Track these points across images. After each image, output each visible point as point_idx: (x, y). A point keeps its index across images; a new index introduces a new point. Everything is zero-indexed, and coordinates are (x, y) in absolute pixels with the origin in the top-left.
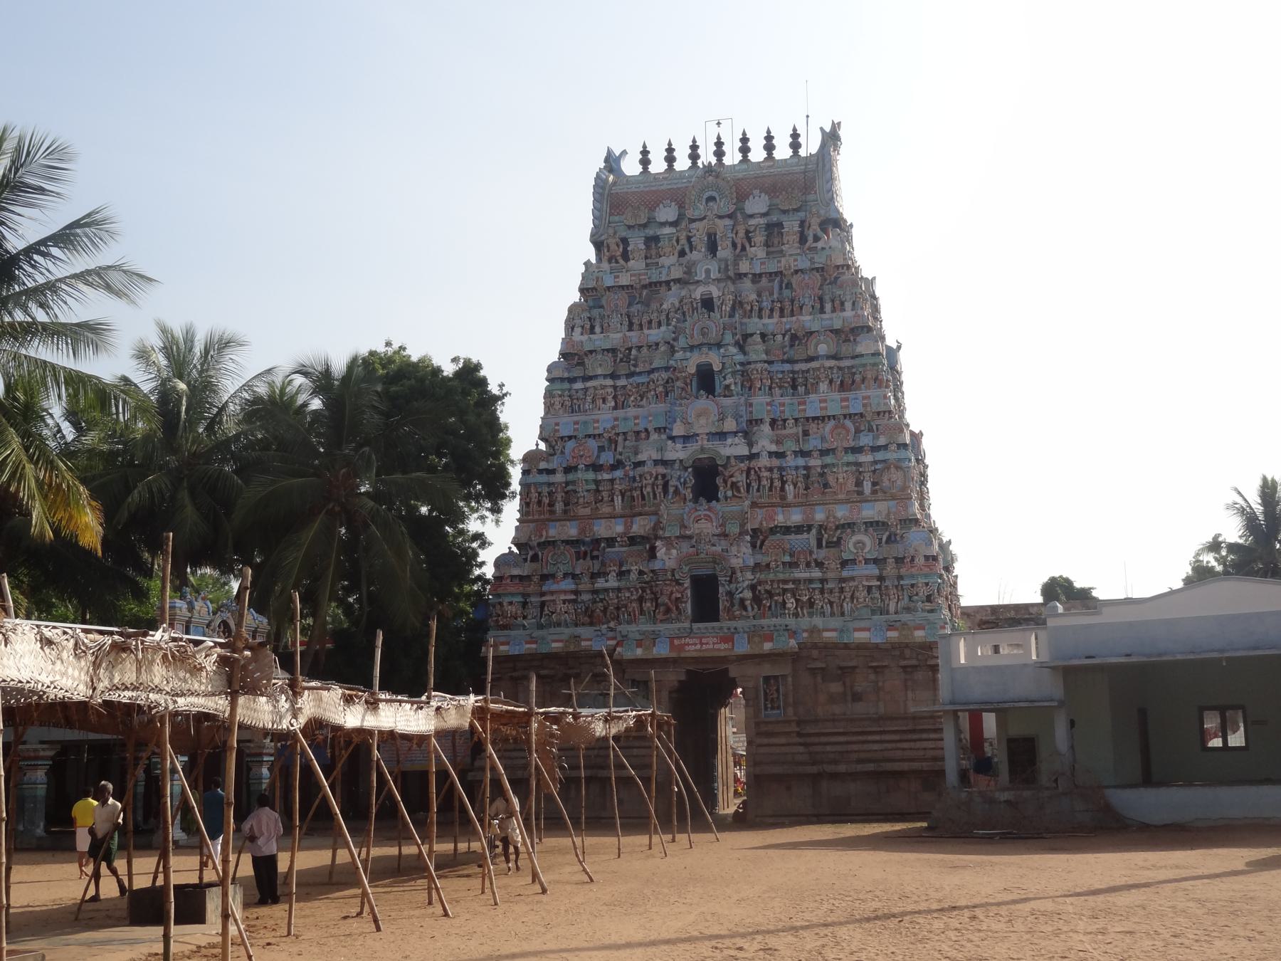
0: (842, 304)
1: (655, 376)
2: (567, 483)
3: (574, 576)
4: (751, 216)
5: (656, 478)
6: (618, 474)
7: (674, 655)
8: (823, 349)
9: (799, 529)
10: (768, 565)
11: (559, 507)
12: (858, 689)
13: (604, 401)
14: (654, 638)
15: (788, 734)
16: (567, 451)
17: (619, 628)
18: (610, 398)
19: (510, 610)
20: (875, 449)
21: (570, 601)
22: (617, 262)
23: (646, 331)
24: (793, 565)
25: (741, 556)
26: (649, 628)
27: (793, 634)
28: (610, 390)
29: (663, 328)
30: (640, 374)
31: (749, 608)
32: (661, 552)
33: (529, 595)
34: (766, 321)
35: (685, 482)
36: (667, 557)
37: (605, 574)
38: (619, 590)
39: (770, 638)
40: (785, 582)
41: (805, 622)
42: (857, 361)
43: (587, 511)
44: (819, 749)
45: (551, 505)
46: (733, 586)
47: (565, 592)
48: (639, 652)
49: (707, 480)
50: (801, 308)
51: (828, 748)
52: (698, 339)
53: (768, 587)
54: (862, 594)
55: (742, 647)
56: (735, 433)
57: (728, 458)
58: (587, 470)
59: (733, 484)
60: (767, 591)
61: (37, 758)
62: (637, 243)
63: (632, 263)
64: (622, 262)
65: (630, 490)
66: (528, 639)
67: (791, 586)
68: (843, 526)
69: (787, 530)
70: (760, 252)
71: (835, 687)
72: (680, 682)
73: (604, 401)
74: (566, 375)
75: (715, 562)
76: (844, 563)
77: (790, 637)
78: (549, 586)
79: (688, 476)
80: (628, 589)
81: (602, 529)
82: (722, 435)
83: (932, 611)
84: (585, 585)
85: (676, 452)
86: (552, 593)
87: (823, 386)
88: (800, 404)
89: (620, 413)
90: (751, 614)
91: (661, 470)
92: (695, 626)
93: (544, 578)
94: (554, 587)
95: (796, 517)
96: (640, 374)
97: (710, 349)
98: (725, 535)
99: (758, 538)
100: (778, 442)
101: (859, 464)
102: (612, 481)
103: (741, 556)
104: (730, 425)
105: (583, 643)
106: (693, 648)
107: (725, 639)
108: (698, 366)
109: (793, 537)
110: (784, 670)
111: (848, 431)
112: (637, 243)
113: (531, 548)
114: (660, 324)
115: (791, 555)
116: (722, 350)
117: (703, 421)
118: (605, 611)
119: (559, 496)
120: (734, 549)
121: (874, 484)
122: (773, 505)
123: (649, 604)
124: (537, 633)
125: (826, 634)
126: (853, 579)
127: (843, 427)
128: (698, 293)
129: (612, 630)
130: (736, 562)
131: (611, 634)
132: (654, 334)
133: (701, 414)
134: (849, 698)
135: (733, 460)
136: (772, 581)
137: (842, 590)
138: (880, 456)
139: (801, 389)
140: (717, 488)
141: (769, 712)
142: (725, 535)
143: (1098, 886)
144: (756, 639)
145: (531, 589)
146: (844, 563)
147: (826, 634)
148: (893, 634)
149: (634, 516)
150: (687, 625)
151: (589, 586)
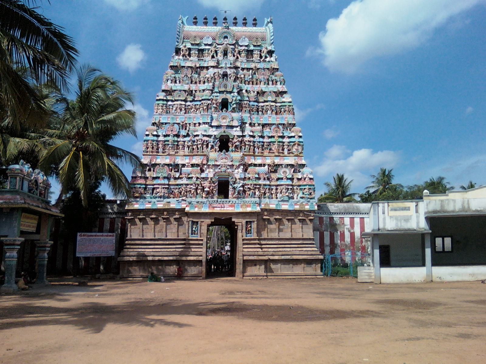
2: (165, 141)
4: (241, 46)
6: (187, 139)
9: (260, 165)
13: (181, 110)
18: (183, 109)
21: (166, 188)
23: (198, 85)
24: (259, 179)
25: (238, 173)
28: (183, 106)
29: (206, 84)
30: (197, 101)
33: (147, 185)
34: (247, 85)
36: (209, 173)
40: (256, 185)
44: (140, 250)
45: (158, 149)
46: (236, 185)
51: (270, 250)
52: (222, 89)
53: (249, 186)
56: (237, 127)
57: (234, 136)
59: (236, 146)
60: (249, 188)
61: (14, 245)
63: (192, 58)
64: (188, 57)
65: (192, 146)
67: (258, 186)
68: (276, 165)
69: (255, 165)
70: (244, 60)
73: (181, 110)
74: (165, 98)
75: (229, 176)
81: (179, 161)
82: (232, 127)
87: (269, 112)
90: (242, 196)
91: (206, 139)
95: (259, 161)
96: (197, 101)
97: (227, 93)
100: (253, 132)
102: (184, 142)
103: (238, 173)
104: (235, 123)
113: (148, 166)
114: (204, 82)
116: (232, 94)
120: (236, 171)
121: (289, 150)
126: (282, 185)
128: (221, 72)
129: (183, 200)
130: (238, 176)
132: (202, 87)
135: (236, 137)
137: (277, 189)
138: (292, 140)
139: (260, 113)
140: (228, 147)
144: (244, 206)
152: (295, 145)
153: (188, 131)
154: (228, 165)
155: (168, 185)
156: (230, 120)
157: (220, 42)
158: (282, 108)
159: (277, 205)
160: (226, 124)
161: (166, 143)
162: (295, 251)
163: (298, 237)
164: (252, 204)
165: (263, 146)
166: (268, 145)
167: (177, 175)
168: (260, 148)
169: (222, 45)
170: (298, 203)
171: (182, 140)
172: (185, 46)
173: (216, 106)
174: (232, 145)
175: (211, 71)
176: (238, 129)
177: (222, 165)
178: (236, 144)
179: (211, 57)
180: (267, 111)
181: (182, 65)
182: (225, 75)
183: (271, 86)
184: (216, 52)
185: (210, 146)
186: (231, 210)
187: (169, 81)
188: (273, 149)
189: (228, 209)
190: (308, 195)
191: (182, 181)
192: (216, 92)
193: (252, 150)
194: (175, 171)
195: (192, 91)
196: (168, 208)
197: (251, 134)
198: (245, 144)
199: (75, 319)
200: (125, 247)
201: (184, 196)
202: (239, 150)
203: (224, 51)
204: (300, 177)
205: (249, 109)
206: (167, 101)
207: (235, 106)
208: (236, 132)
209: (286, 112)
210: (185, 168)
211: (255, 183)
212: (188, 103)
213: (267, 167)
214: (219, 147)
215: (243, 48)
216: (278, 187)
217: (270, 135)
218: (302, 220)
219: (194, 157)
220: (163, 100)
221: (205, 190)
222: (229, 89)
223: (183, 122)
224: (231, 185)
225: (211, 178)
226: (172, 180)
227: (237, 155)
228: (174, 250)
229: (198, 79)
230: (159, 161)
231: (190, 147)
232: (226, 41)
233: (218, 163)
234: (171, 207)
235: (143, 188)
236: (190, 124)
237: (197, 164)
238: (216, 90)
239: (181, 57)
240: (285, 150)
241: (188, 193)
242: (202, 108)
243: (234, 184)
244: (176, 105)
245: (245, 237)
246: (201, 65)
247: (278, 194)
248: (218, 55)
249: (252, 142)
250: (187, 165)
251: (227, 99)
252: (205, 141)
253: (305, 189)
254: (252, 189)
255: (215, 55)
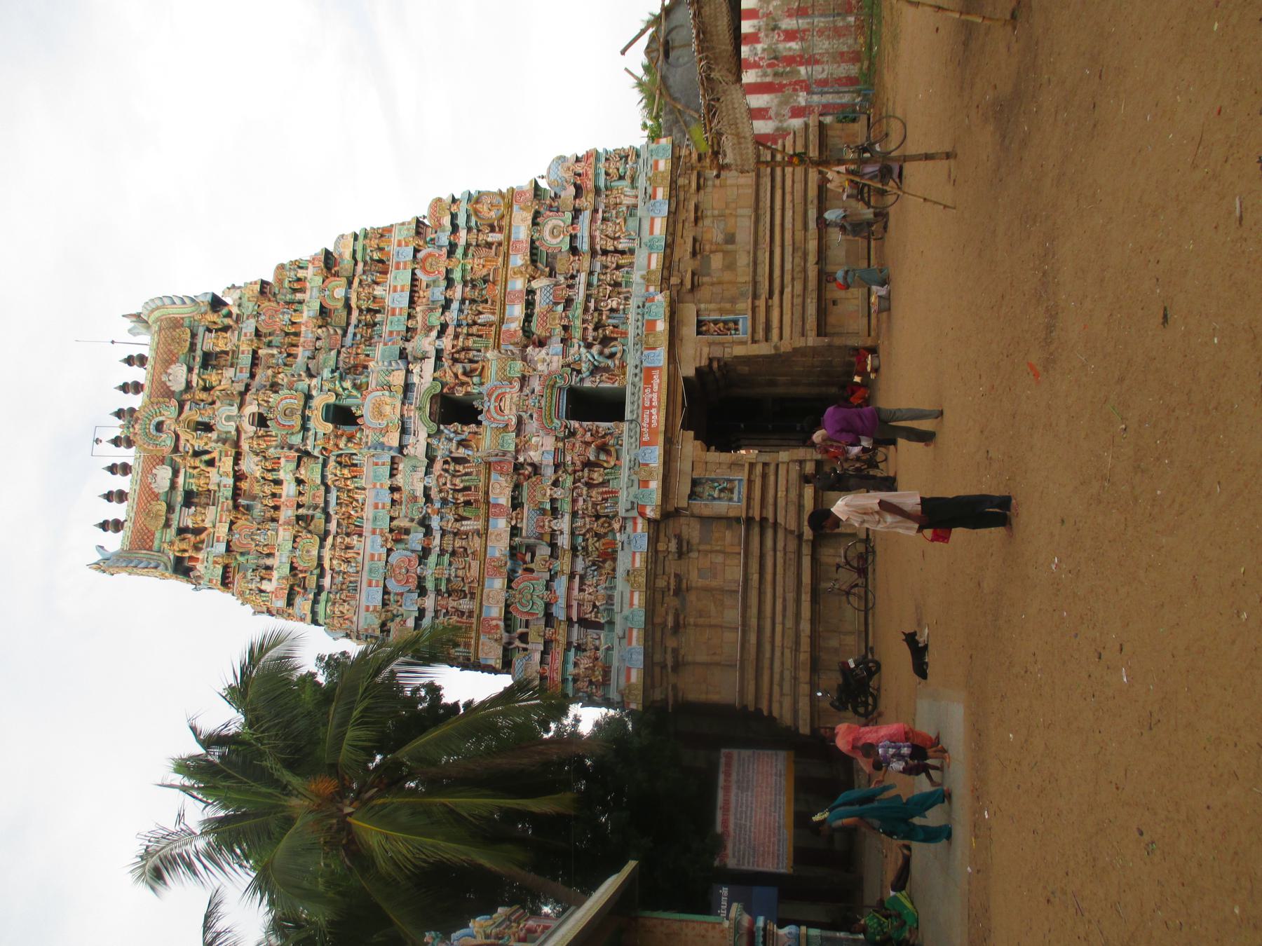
0: (299, 280)
1: (330, 479)
2: (438, 592)
3: (552, 578)
5: (446, 471)
6: (435, 523)
7: (661, 438)
8: (340, 293)
9: (530, 304)
10: (565, 328)
11: (465, 605)
12: (720, 238)
13: (348, 547)
14: (636, 464)
15: (768, 309)
16: (399, 590)
17: (622, 513)
18: (347, 540)
19: (585, 663)
20: (455, 228)
22: (203, 542)
25: (548, 359)
26: (624, 474)
27: (649, 299)
31: (613, 350)
32: (534, 456)
35: (455, 432)
36: (541, 448)
37: (553, 534)
38: (574, 514)
39: (651, 324)
40: (586, 310)
41: (637, 288)
42: (359, 257)
43: (475, 565)
46: (584, 367)
47: (570, 588)
48: (655, 485)
49: (455, 410)
50: (294, 323)
51: (788, 266)
52: (297, 422)
53: (591, 327)
54: (610, 229)
55: (660, 357)
56: (408, 372)
58: (425, 565)
59: (465, 373)
60: (596, 329)
62: (188, 518)
64: (203, 536)
66: (624, 642)
69: (528, 318)
71: (717, 261)
72: (696, 438)
73: (348, 547)
74: (311, 596)
75: (553, 386)
76: (574, 250)
77: (652, 300)
78: (559, 612)
79: (448, 430)
80: (574, 501)
81: (499, 547)
82: (408, 388)
83: (638, 155)
84: (564, 564)
85: (417, 446)
86: (569, 606)
87: (378, 291)
88: (393, 314)
89: (367, 527)
90: (620, 348)
91: (438, 466)
92: (628, 416)
93: (549, 618)
94: (562, 602)
96: (326, 502)
98: (524, 380)
99: (531, 339)
100: (431, 329)
101: (468, 245)
102: (444, 533)
103: (548, 359)
104: (398, 379)
105: (637, 565)
106: (655, 417)
107: (648, 379)
108: (326, 420)
109: (537, 310)
110: (689, 313)
111: (430, 255)
112: (188, 518)
115: (556, 304)
116: (314, 393)
117: (387, 409)
118: (598, 536)
119: (452, 603)
120: (540, 367)
121: (492, 229)
122: (498, 334)
123: (595, 475)
124: (618, 629)
125: (654, 266)
126: (592, 238)
127: (424, 260)
128: (249, 429)
129: (623, 528)
130: (557, 362)
131: (629, 525)
132: (289, 489)
133: (378, 408)
134: (730, 247)
136: (584, 321)
137: (605, 252)
138: (461, 221)
141: (735, 497)
142: (524, 380)
143: (922, 163)
144: (651, 340)
145: (562, 639)
146: (574, 250)
147: (654, 266)
148: (661, 193)
149: (488, 503)
150: (625, 426)
151: (567, 559)
152: (476, 212)
153: (412, 520)
154: (521, 390)
155: (572, 576)
156: (387, 393)
157: (168, 442)
158: (371, 259)
159: (651, 247)
160: (398, 404)
161: (443, 588)
162: (793, 193)
163: (750, 191)
164: (646, 317)
165: (473, 301)
166: (474, 287)
167: (544, 551)
168: (480, 308)
169: (177, 437)
170: (650, 191)
171: (437, 541)
172: (172, 543)
173: (344, 439)
174: (463, 384)
175: (251, 465)
176: (415, 368)
177: (518, 410)
178: (460, 371)
179: (209, 469)
180: (375, 298)
181: (221, 548)
182: (261, 421)
183: (306, 296)
184: (197, 454)
185: (462, 452)
186: (660, 378)
187: (263, 587)
188: (484, 272)
189: (656, 388)
190: (626, 163)
191: (562, 533)
192: (304, 439)
193: (484, 331)
194: (532, 561)
195: (298, 518)
196: (644, 574)
197: (434, 334)
198: (463, 349)
199: (609, 887)
200: (765, 713)
201: (610, 525)
202: (479, 366)
203: (196, 430)
204: (572, 190)
205: (363, 346)
206: (320, 589)
207: (348, 384)
208: (424, 376)
209: (382, 245)
210: (524, 525)
211: (579, 311)
212: (333, 526)
213: (535, 284)
214: (465, 422)
215: (195, 378)
216: (598, 247)
217: (443, 284)
218: (702, 181)
219: (491, 500)
220: (315, 601)
221: (592, 458)
222: (298, 403)
223: (386, 541)
224: (582, 380)
225: (557, 439)
226: (557, 565)
227: (541, 448)
228: (780, 555)
229: (266, 502)
230: (495, 611)
231: (461, 511)
232: (170, 425)
233: (514, 421)
234: (644, 565)
235: (576, 655)
236: (392, 519)
237: (513, 491)
238: (296, 440)
239: (200, 556)
240: (489, 239)
241: (602, 512)
242: (349, 482)
243: (579, 372)
244: (335, 562)
245: (748, 337)
246: (229, 494)
247: (620, 247)
248: (206, 448)
249: (459, 330)
250: (513, 523)
251: (328, 406)
252: (446, 466)
253: (607, 174)
254: (600, 320)
255: (206, 457)
